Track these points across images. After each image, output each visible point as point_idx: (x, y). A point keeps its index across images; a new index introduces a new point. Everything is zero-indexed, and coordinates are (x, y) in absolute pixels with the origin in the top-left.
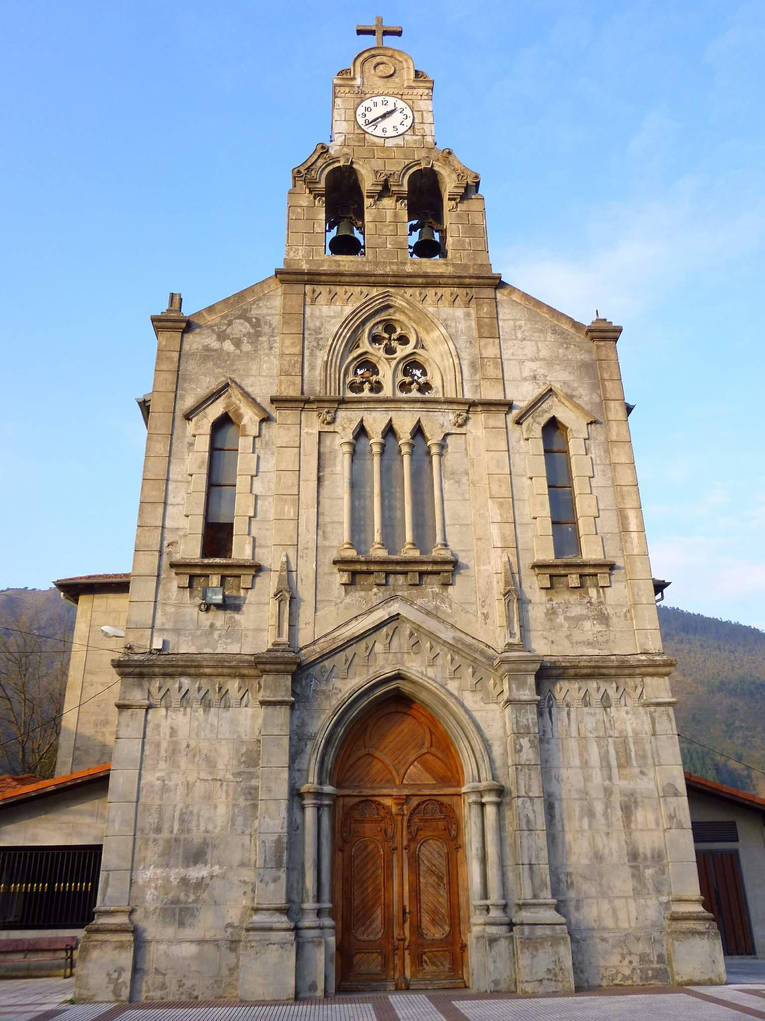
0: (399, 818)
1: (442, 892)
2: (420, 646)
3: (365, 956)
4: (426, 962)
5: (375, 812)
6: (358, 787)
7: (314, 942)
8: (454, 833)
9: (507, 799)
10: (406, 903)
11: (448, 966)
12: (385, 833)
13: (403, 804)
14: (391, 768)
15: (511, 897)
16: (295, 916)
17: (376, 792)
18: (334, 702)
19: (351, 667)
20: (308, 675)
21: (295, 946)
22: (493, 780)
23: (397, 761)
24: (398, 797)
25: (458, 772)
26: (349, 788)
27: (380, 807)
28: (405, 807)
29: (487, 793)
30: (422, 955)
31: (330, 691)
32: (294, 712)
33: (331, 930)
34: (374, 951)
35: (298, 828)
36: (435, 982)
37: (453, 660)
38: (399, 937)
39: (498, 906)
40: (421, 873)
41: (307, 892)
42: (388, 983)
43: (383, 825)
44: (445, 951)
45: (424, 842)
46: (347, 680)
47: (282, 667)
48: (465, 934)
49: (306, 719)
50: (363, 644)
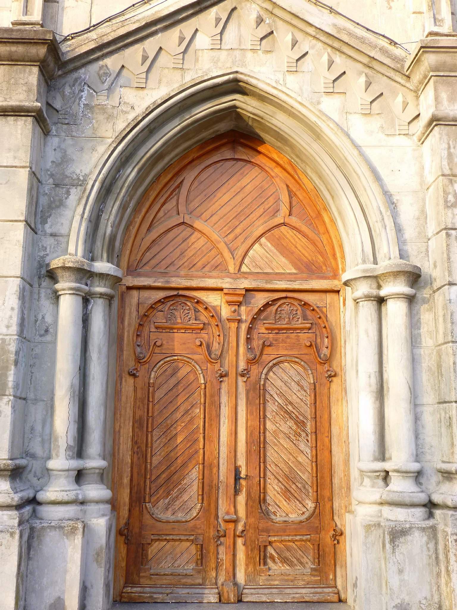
0: (234, 325)
1: (302, 446)
2: (274, 41)
3: (169, 546)
4: (272, 558)
5: (192, 314)
6: (164, 274)
7: (61, 528)
8: (325, 352)
9: (426, 293)
10: (242, 462)
11: (310, 565)
12: (208, 347)
13: (240, 304)
14: (222, 246)
15: (428, 457)
16: (34, 480)
17: (194, 283)
18: (121, 125)
19: (154, 70)
20: (76, 80)
21: (17, 536)
22: (401, 258)
23: (231, 236)
24: (232, 292)
25: (334, 255)
26: (147, 275)
27: (201, 308)
28: (243, 308)
29: (392, 278)
30: (265, 547)
31: (114, 107)
32: (49, 138)
33: (102, 506)
34: (183, 538)
35: (47, 331)
36: (288, 591)
37: (331, 63)
38: (227, 517)
39: (407, 472)
40: (269, 415)
41: (56, 440)
42: (206, 591)
43: (204, 335)
44: (305, 541)
45: (275, 365)
46: (145, 91)
47: (19, 49)
48: (340, 516)
49: (69, 151)
50: (174, 33)
